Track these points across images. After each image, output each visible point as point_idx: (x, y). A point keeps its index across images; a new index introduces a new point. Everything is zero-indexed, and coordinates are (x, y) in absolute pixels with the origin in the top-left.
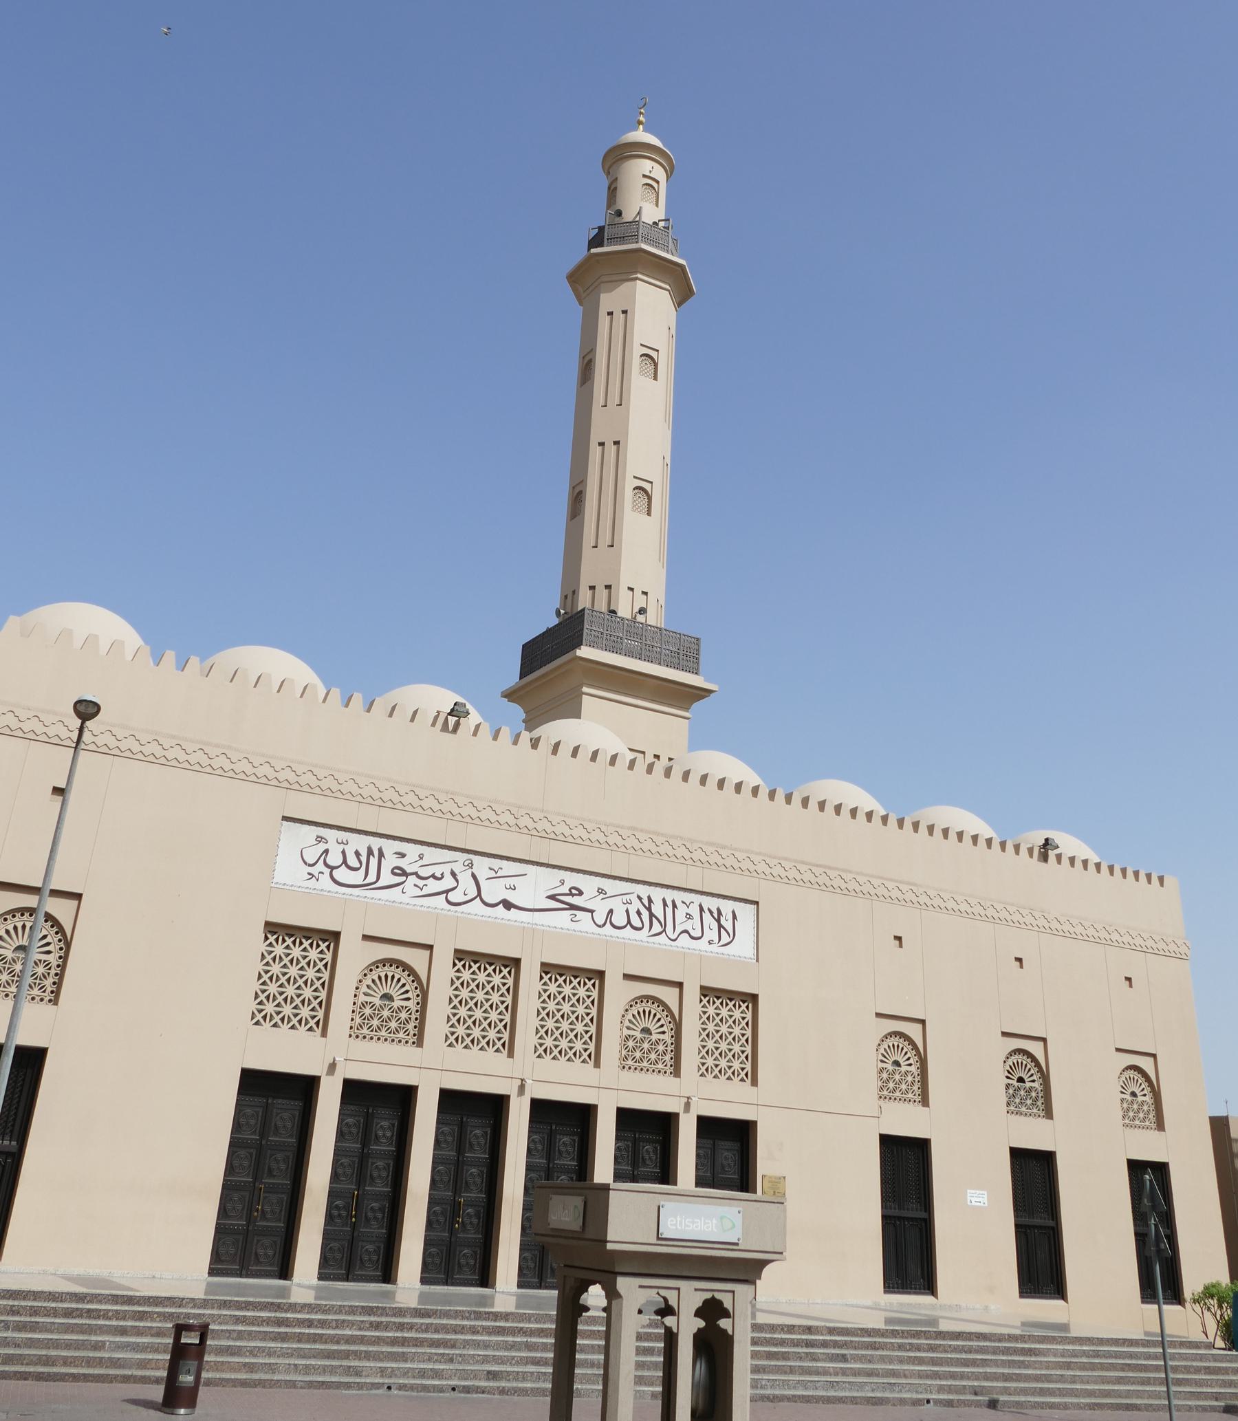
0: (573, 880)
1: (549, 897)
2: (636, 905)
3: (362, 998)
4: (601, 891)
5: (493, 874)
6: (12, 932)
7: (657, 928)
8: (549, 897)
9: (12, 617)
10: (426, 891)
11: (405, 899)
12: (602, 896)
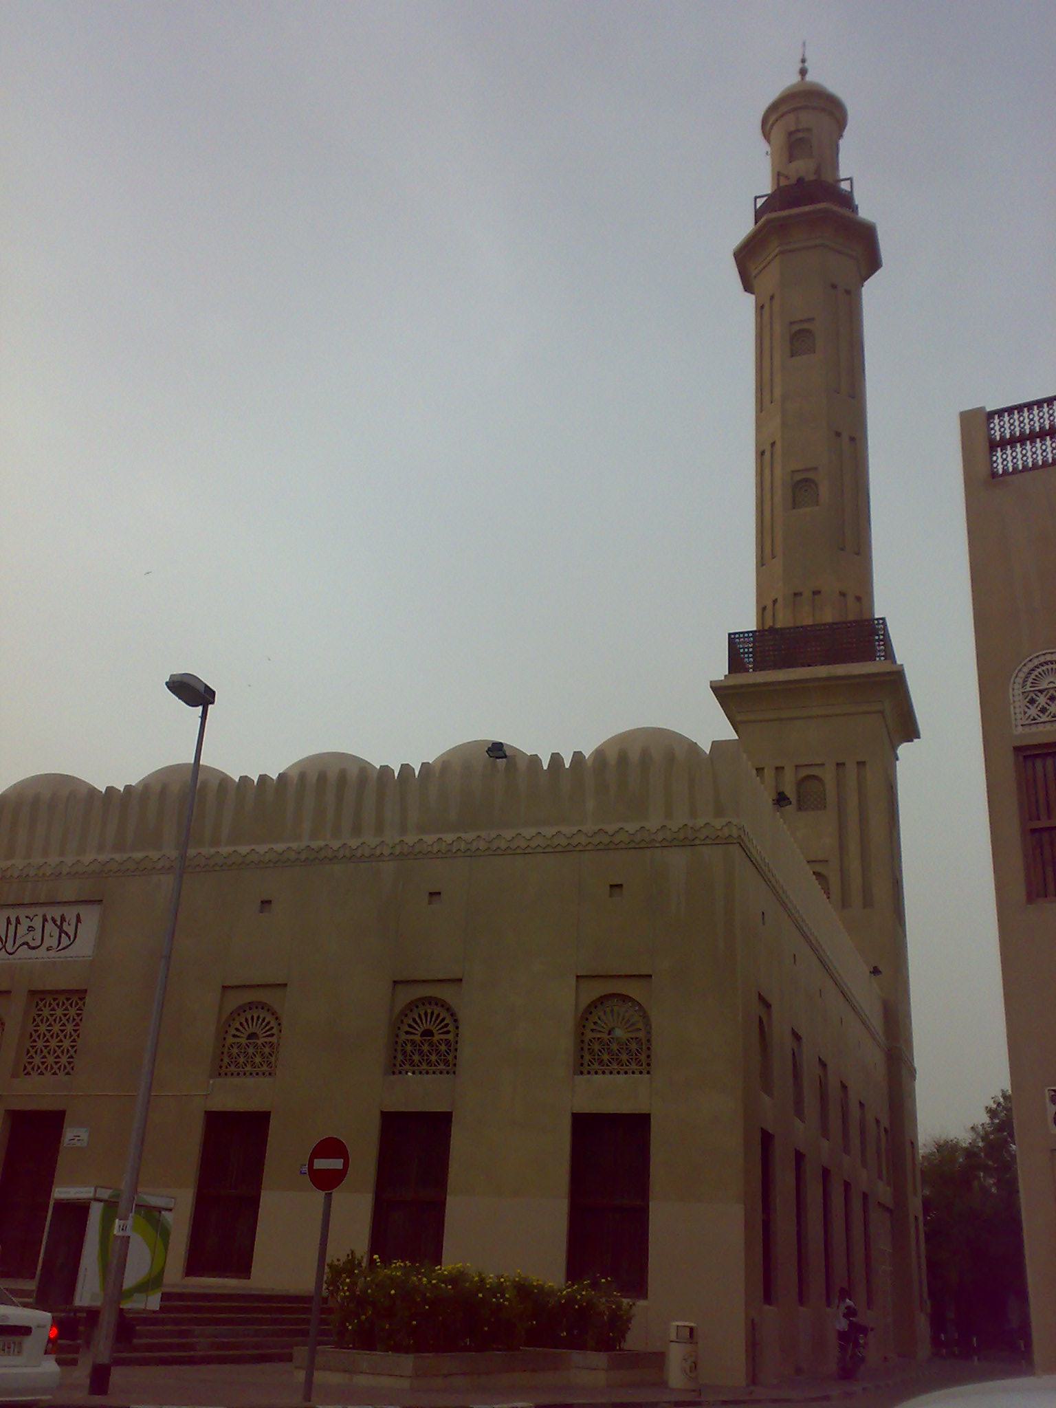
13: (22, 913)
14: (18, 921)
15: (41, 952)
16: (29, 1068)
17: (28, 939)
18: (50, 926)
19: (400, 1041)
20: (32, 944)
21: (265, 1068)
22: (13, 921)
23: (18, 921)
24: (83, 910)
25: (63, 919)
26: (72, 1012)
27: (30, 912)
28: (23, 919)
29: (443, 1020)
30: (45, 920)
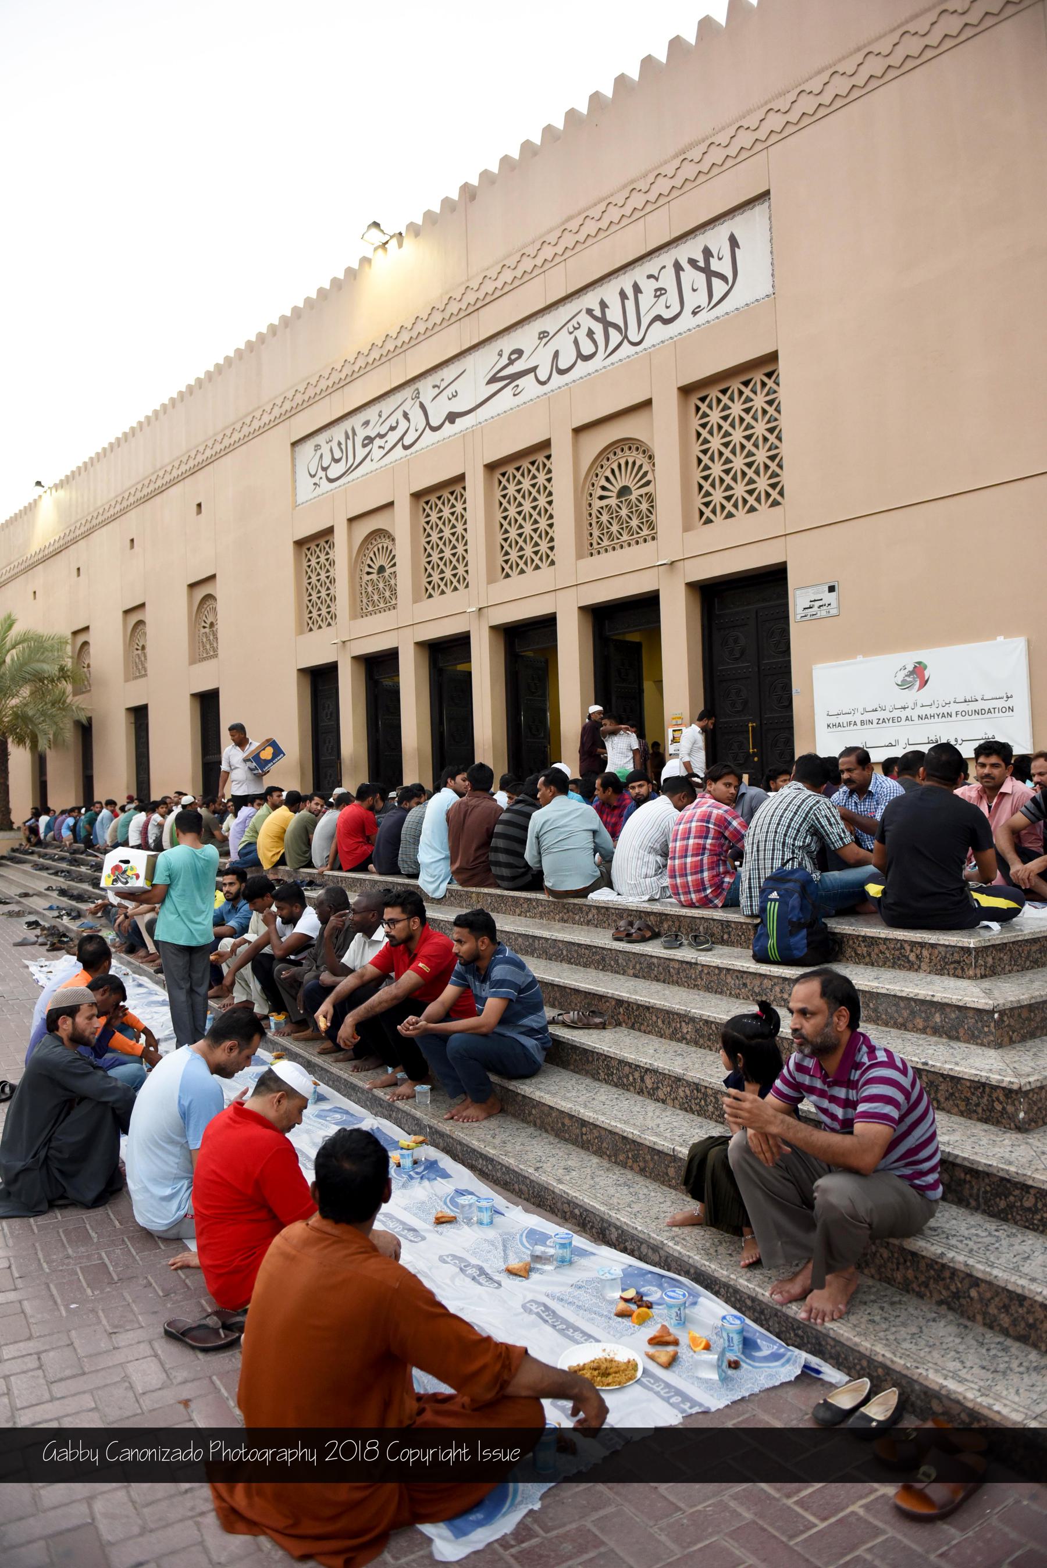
0: (507, 344)
1: (488, 383)
2: (587, 322)
3: (597, 504)
4: (543, 335)
5: (437, 391)
6: (607, 485)
7: (615, 337)
8: (488, 383)
9: (244, 808)
10: (388, 447)
11: (374, 466)
12: (545, 340)
13: (638, 274)
14: (637, 290)
15: (686, 321)
16: (707, 512)
17: (660, 310)
18: (690, 275)
19: (594, 512)
20: (667, 315)
21: (645, 532)
22: (630, 292)
23: (637, 290)
24: (735, 226)
25: (707, 253)
26: (759, 401)
27: (651, 266)
28: (644, 284)
29: (641, 466)
30: (678, 267)
